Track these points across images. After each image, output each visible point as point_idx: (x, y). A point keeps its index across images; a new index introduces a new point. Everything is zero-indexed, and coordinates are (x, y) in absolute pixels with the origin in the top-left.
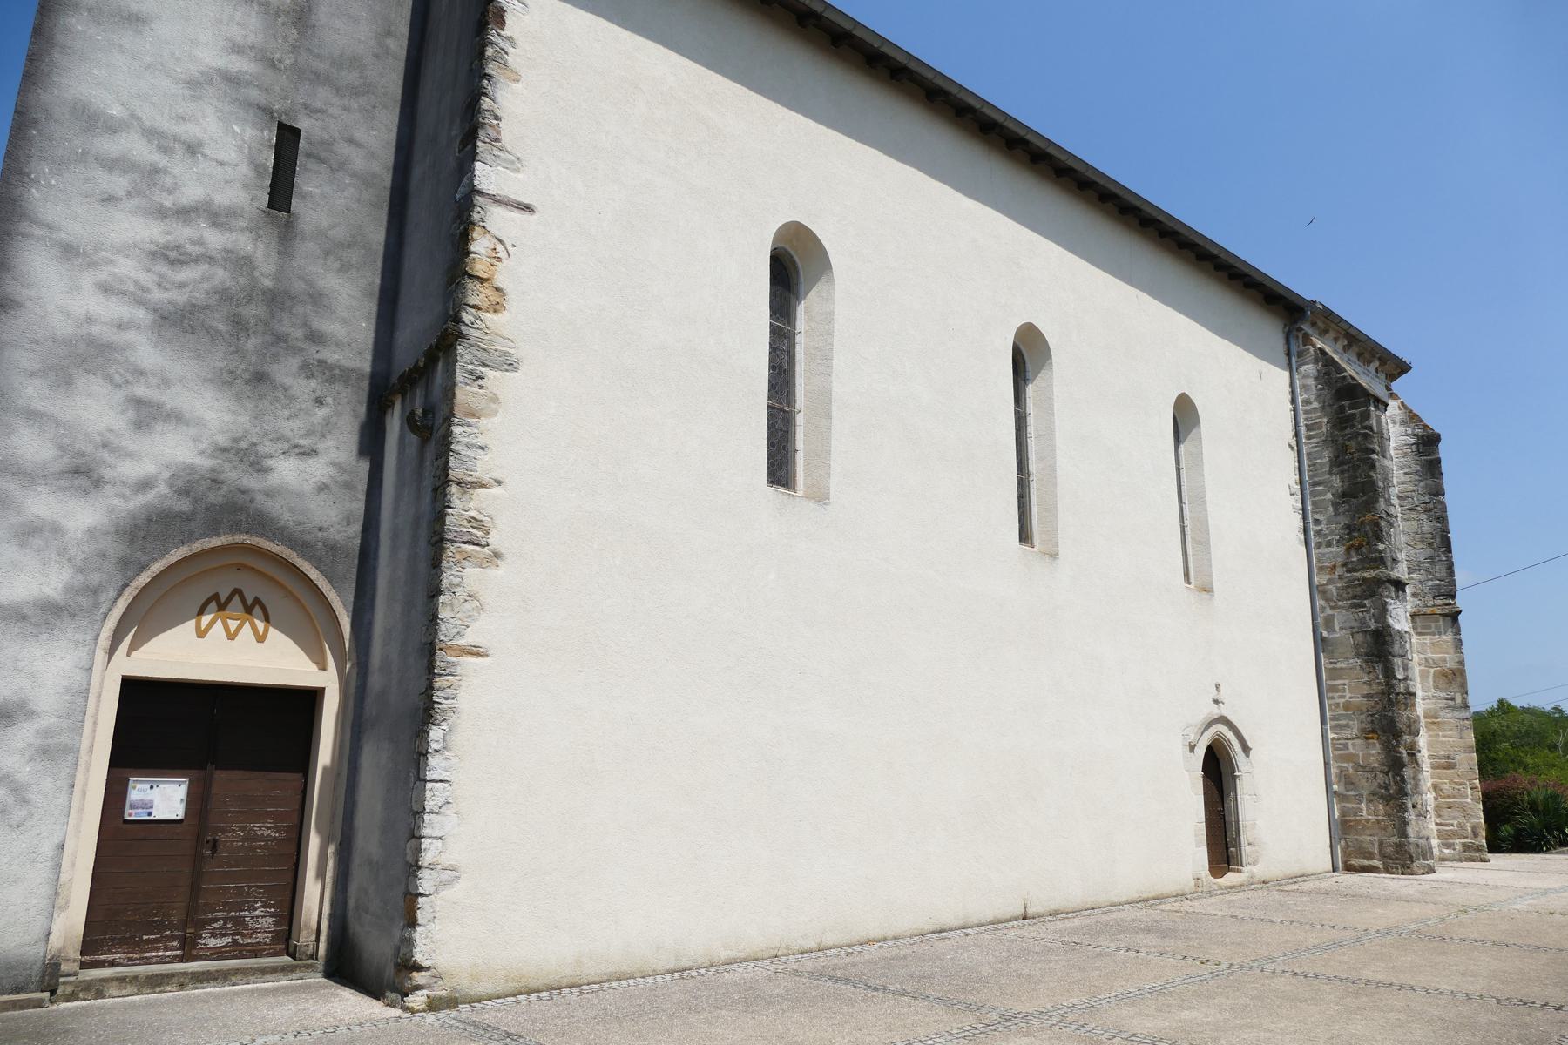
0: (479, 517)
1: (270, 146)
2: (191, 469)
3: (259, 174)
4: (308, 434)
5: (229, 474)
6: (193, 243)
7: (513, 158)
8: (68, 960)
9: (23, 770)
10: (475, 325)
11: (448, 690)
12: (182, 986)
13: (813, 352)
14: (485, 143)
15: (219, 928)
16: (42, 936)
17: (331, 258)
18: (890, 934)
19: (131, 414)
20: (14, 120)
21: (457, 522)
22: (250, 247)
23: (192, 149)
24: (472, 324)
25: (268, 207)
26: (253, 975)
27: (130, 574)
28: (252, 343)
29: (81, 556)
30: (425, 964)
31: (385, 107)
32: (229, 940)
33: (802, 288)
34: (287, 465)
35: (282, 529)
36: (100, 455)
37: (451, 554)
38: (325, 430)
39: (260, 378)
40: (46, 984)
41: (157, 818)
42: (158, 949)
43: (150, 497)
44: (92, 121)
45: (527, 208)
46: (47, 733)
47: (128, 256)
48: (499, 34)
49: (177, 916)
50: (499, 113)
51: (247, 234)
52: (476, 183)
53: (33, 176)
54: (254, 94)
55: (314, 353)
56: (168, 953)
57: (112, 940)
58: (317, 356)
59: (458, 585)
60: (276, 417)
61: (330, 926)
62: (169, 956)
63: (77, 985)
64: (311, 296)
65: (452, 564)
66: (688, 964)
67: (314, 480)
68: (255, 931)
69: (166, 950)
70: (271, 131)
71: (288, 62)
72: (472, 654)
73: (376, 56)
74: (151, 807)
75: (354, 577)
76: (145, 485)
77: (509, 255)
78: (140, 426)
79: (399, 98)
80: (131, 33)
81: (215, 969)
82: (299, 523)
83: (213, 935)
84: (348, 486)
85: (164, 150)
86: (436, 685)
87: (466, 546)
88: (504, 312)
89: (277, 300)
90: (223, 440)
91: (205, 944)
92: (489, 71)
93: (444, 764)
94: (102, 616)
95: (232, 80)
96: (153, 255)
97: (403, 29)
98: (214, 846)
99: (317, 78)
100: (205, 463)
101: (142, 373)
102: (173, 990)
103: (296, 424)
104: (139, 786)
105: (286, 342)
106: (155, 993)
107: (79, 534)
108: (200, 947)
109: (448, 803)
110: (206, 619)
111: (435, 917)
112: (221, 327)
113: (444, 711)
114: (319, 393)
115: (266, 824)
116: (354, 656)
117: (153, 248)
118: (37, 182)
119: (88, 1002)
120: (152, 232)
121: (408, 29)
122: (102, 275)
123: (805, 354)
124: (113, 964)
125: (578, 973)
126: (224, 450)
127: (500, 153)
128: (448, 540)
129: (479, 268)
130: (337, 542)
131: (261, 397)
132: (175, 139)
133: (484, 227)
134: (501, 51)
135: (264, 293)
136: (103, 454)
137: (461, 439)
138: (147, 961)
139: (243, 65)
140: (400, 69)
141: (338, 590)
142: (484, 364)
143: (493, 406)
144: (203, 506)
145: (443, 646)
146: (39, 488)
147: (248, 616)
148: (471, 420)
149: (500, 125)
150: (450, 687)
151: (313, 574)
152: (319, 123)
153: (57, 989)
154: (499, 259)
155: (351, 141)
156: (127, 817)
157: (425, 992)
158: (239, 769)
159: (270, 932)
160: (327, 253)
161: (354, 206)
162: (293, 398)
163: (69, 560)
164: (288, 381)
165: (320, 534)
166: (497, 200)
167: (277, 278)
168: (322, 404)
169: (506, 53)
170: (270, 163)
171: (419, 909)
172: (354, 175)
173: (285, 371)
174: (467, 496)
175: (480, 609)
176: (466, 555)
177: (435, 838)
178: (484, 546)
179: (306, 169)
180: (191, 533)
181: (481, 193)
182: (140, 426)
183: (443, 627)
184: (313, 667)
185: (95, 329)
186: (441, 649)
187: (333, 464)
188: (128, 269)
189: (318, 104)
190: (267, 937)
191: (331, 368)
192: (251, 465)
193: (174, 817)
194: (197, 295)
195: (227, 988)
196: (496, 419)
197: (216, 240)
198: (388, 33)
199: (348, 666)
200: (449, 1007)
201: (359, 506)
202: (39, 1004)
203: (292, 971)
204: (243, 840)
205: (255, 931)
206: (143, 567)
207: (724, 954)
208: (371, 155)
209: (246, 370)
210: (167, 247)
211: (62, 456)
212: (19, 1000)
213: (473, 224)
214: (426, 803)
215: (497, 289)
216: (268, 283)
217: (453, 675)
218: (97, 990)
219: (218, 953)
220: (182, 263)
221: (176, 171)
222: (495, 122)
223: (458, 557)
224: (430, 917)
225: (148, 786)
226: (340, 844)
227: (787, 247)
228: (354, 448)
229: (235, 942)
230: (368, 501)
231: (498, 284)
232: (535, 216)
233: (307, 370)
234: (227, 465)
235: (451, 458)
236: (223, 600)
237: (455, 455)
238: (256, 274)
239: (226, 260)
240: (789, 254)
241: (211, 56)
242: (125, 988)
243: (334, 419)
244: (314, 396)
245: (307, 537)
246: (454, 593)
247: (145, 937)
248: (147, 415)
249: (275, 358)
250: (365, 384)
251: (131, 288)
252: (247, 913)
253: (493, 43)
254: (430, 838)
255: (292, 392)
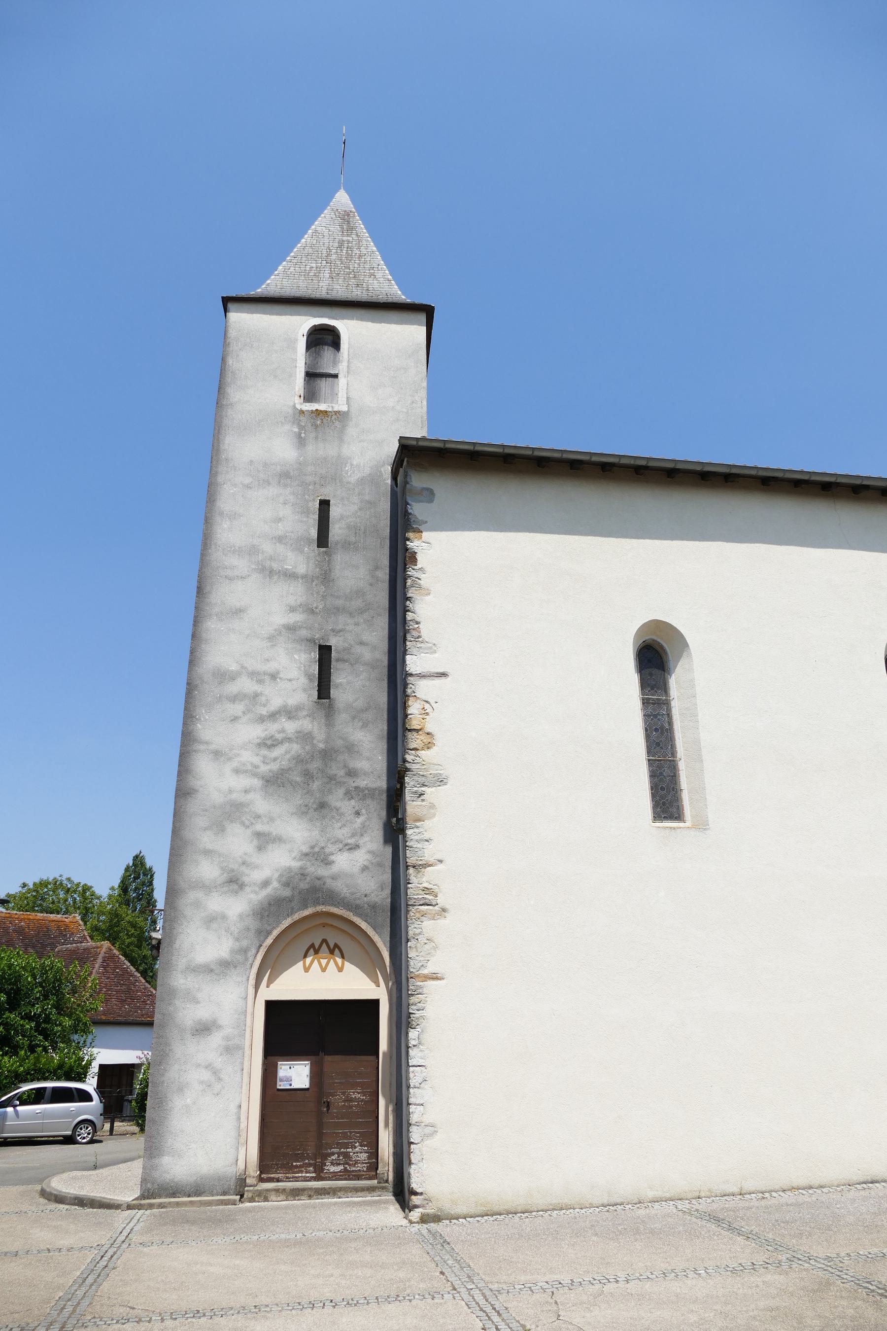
0: (430, 886)
1: (316, 662)
2: (290, 869)
3: (311, 680)
4: (353, 835)
5: (310, 869)
6: (279, 732)
7: (431, 645)
8: (250, 1177)
9: (218, 1061)
10: (416, 761)
11: (419, 1004)
12: (310, 1197)
13: (684, 712)
14: (411, 641)
15: (335, 1160)
16: (234, 1161)
17: (357, 720)
18: (815, 1182)
19: (255, 842)
20: (186, 688)
21: (414, 892)
22: (310, 726)
23: (274, 677)
24: (413, 761)
25: (318, 699)
26: (351, 1192)
27: (262, 938)
28: (316, 785)
29: (236, 931)
30: (419, 1190)
31: (379, 615)
32: (341, 1167)
33: (671, 664)
34: (342, 857)
35: (343, 899)
36: (241, 869)
37: (412, 914)
38: (363, 830)
39: (322, 806)
40: (238, 1191)
41: (295, 1087)
42: (302, 1172)
43: (269, 890)
44: (223, 676)
45: (443, 675)
46: (227, 1038)
47: (246, 749)
48: (413, 569)
49: (311, 1151)
50: (418, 619)
51: (308, 718)
52: (407, 669)
53: (197, 717)
54: (304, 633)
55: (352, 783)
56: (308, 1175)
57: (277, 1165)
58: (354, 785)
59: (420, 934)
60: (333, 828)
61: (394, 1161)
62: (308, 1177)
63: (254, 1192)
64: (347, 747)
65: (415, 921)
66: (619, 1201)
67: (359, 864)
68: (356, 1162)
69: (306, 1172)
70: (315, 652)
71: (321, 607)
72: (433, 979)
73: (371, 585)
74: (291, 1080)
75: (389, 924)
76: (266, 884)
77: (434, 709)
78: (260, 848)
79: (387, 606)
80: (237, 620)
81: (328, 1186)
82: (352, 894)
83: (332, 1164)
84: (380, 865)
85: (260, 682)
86: (411, 1002)
87: (423, 907)
88: (434, 747)
89: (327, 755)
90: (305, 849)
91: (328, 1170)
92: (409, 595)
93: (420, 1054)
94: (250, 966)
95: (291, 628)
96: (259, 745)
97: (385, 562)
98: (328, 1105)
99: (337, 610)
100: (296, 864)
101: (259, 817)
102: (305, 1199)
103: (346, 831)
104: (283, 1067)
105: (335, 780)
106: (295, 1200)
107: (235, 918)
108: (325, 1171)
109: (426, 1080)
110: (308, 960)
111: (423, 1159)
112: (298, 779)
113: (417, 1018)
114: (357, 808)
115: (357, 1090)
116: (393, 977)
117: (259, 741)
118: (199, 719)
119: (260, 1203)
120: (257, 732)
121: (388, 561)
122: (235, 764)
123: (680, 715)
124: (278, 1180)
125: (530, 1202)
126: (306, 855)
127: (422, 645)
128: (410, 905)
129: (414, 723)
130: (376, 903)
131: (324, 818)
132: (265, 673)
133: (415, 696)
134: (416, 579)
135: (320, 752)
136: (243, 869)
137: (413, 838)
138: (296, 1179)
139: (297, 617)
140: (386, 587)
141: (380, 934)
142: (424, 785)
143: (433, 811)
144: (298, 891)
145: (413, 975)
146: (213, 894)
147: (331, 955)
148: (418, 824)
149: (420, 627)
150: (420, 1002)
151: (364, 925)
152: (341, 639)
153: (244, 1194)
154: (427, 714)
155: (362, 643)
156: (278, 1087)
157: (420, 1210)
158: (338, 1055)
159: (366, 1163)
160: (354, 718)
161: (367, 684)
162: (342, 814)
163: (231, 934)
164: (338, 804)
165: (365, 899)
166: (422, 676)
167: (326, 742)
168: (360, 815)
169: (420, 579)
170: (317, 672)
171: (412, 1152)
172: (365, 664)
173: (336, 799)
174: (421, 874)
175: (435, 948)
176: (423, 913)
177: (418, 1105)
178: (435, 905)
179: (337, 669)
180: (292, 909)
181: (411, 675)
182: (260, 848)
183: (412, 963)
184: (373, 986)
185: (234, 796)
186: (412, 978)
187: (369, 852)
188: (248, 757)
189: (340, 627)
190: (364, 1167)
191: (363, 790)
192: (322, 861)
193: (304, 1087)
194: (283, 763)
195: (335, 1200)
196: (435, 820)
197: (291, 727)
198: (377, 568)
199: (390, 984)
200: (434, 1222)
201: (387, 877)
202: (234, 1203)
203: (373, 1191)
204: (344, 1101)
205: (356, 1162)
206: (269, 933)
207: (651, 1194)
208: (374, 648)
209: (314, 803)
210: (265, 739)
211: (223, 873)
212: (224, 1200)
213: (408, 696)
214: (410, 1081)
215: (428, 734)
216: (321, 746)
217: (421, 994)
218: (264, 1196)
219: (335, 1176)
220: (273, 746)
221: (266, 692)
222: (417, 626)
223: (418, 915)
224: (420, 1158)
225: (289, 1067)
226: (396, 1104)
227: (655, 638)
228: (381, 840)
229: (345, 1169)
230: (393, 873)
231: (427, 730)
232: (449, 679)
233: (349, 795)
234: (308, 863)
235: (407, 851)
236: (317, 947)
237: (410, 849)
238: (315, 742)
239: (297, 738)
240: (656, 641)
241: (281, 618)
242: (279, 1196)
243: (367, 823)
244: (354, 810)
245: (358, 902)
246: (417, 939)
247: (294, 1164)
248: (264, 841)
249: (330, 791)
250: (384, 797)
251: (250, 768)
252: (351, 1150)
253: (410, 576)
254: (415, 1104)
255: (342, 811)
